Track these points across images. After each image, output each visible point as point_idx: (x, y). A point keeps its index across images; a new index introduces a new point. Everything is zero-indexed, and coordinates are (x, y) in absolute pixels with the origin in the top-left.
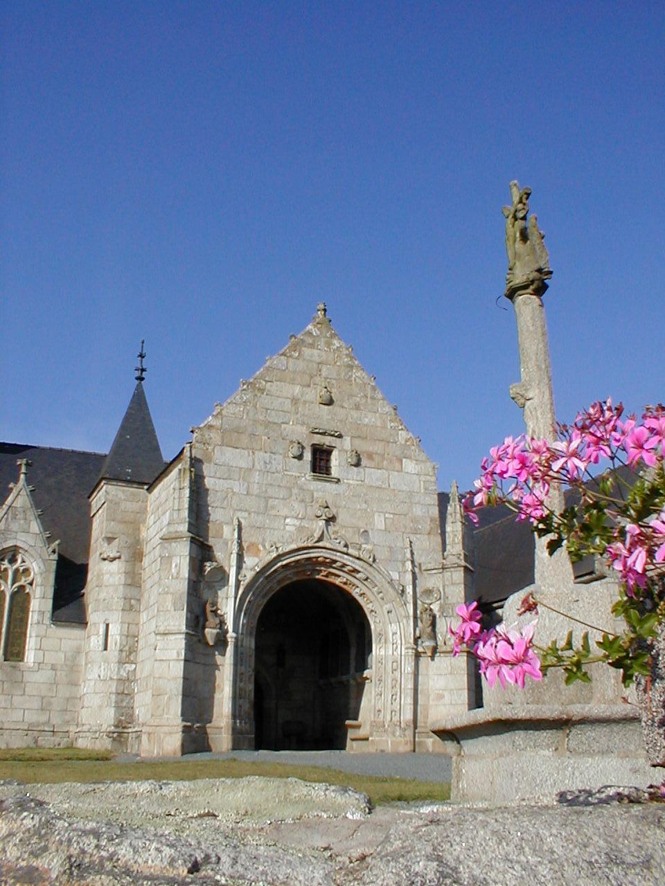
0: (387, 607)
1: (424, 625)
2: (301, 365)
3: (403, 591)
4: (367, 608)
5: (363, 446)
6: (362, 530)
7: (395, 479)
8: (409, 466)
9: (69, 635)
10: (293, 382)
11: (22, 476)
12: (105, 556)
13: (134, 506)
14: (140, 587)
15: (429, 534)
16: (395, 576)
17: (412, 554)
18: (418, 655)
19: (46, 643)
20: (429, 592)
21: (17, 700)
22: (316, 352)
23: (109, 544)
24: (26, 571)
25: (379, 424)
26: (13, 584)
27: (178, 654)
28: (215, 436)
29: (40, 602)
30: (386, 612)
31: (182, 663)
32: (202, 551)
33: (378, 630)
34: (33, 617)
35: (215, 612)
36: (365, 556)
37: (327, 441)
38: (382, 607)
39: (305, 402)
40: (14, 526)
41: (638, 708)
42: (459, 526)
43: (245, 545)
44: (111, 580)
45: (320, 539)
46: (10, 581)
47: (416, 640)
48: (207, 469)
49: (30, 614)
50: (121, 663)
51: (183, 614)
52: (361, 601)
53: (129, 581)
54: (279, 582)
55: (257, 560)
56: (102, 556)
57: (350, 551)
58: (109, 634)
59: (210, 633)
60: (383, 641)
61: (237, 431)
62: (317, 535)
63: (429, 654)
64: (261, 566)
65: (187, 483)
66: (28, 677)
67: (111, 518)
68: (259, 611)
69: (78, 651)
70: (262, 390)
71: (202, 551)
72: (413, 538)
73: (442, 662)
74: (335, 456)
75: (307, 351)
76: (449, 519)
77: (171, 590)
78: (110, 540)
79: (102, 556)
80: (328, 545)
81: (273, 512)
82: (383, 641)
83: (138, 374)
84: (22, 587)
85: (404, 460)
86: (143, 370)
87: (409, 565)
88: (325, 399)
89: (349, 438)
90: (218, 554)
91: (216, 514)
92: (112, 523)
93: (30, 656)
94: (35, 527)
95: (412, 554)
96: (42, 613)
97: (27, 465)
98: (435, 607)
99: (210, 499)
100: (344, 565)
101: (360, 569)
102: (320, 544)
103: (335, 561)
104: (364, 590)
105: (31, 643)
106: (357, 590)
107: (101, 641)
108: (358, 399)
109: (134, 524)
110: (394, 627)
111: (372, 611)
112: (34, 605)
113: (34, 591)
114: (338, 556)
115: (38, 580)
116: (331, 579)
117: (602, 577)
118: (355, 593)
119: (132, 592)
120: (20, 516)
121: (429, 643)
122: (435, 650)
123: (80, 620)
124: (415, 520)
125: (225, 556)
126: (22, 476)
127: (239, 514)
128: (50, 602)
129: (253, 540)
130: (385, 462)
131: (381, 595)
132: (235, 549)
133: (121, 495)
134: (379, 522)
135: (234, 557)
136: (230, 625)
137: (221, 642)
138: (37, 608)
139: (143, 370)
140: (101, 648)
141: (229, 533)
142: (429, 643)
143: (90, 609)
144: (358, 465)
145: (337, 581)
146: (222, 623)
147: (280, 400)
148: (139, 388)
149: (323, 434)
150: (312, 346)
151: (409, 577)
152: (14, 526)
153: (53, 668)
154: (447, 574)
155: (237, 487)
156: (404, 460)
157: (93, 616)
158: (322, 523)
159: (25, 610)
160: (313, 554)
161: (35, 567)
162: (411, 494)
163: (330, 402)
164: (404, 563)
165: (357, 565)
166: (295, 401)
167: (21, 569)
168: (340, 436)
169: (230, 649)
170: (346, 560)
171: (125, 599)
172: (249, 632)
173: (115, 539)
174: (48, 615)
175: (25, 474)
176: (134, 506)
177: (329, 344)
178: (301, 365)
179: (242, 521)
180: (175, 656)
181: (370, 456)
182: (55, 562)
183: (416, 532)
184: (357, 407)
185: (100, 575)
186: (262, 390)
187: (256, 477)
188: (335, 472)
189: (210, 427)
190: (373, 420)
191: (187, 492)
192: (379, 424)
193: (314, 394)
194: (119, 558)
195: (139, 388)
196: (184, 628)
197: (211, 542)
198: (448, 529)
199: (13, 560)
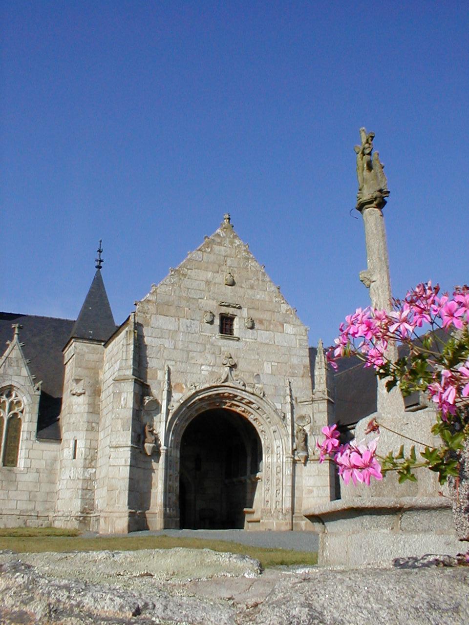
0: (273, 428)
1: (299, 441)
2: (212, 257)
3: (284, 417)
4: (259, 429)
5: (256, 315)
6: (255, 374)
7: (278, 338)
8: (289, 328)
9: (49, 448)
10: (206, 269)
11: (16, 336)
12: (74, 392)
13: (94, 357)
14: (99, 414)
15: (303, 376)
16: (279, 406)
17: (291, 391)
18: (295, 462)
19: (33, 454)
20: (302, 418)
21: (12, 494)
22: (223, 248)
23: (77, 384)
24: (19, 403)
25: (267, 299)
26: (9, 412)
27: (126, 461)
28: (152, 308)
29: (28, 424)
30: (272, 432)
31: (128, 468)
32: (142, 389)
33: (267, 444)
34: (23, 436)
35: (151, 432)
36: (257, 392)
37: (231, 311)
38: (269, 428)
39: (215, 284)
40: (10, 371)
42: (324, 371)
43: (173, 384)
44: (78, 409)
45: (226, 380)
46: (7, 410)
47: (293, 451)
48: (146, 331)
49: (21, 433)
50: (85, 467)
51: (129, 433)
52: (255, 424)
53: (91, 410)
54: (197, 410)
55: (181, 395)
56: (72, 392)
57: (247, 389)
58: (77, 447)
59: (148, 447)
60: (270, 452)
61: (167, 304)
62: (223, 378)
63: (303, 461)
64: (184, 399)
65: (132, 341)
66: (20, 478)
67: (78, 365)
68: (183, 431)
69: (55, 460)
70: (185, 275)
71: (142, 389)
72: (292, 380)
73: (312, 467)
74: (236, 322)
75: (216, 248)
76: (317, 366)
77: (121, 416)
78: (77, 381)
79: (72, 392)
80: (231, 385)
81: (193, 361)
82: (270, 452)
83: (97, 264)
84: (15, 414)
86: (101, 261)
87: (288, 399)
89: (246, 309)
90: (154, 391)
91: (153, 363)
92: (79, 369)
93: (21, 463)
94: (25, 371)
95: (291, 391)
96: (29, 432)
97: (19, 328)
98: (307, 429)
99: (148, 352)
100: (243, 399)
101: (254, 401)
102: (226, 384)
103: (236, 396)
104: (257, 416)
105: (22, 454)
106: (252, 416)
107: (71, 452)
108: (253, 282)
109: (95, 370)
110: (278, 443)
111: (262, 431)
112: (24, 427)
113: (24, 417)
114: (238, 392)
115: (27, 409)
116: (234, 409)
117: (425, 407)
118: (251, 418)
119: (93, 418)
120: (14, 364)
121: (303, 454)
122: (307, 459)
123: (56, 438)
124: (293, 367)
125: (159, 392)
126: (16, 336)
127: (168, 363)
128: (35, 425)
129: (179, 381)
130: (272, 326)
131: (269, 419)
132: (166, 387)
133: (85, 349)
134: (267, 368)
135: (165, 393)
136: (162, 441)
137: (156, 453)
138: (26, 429)
139: (101, 261)
140: (71, 457)
141: (162, 376)
142: (303, 454)
143: (63, 430)
144: (252, 328)
145: (238, 410)
146: (157, 440)
147: (197, 282)
148: (98, 274)
149: (228, 306)
150: (220, 244)
151: (289, 407)
152: (10, 371)
153: (38, 471)
154: (315, 405)
155: (167, 344)
156: (285, 325)
157: (66, 435)
158: (227, 369)
159: (18, 430)
160: (221, 391)
161: (25, 400)
162: (290, 348)
164: (285, 397)
165: (252, 398)
166: (208, 283)
167: (15, 401)
168: (240, 308)
169: (162, 458)
170: (244, 395)
171: (88, 422)
173: (81, 380)
174: (34, 434)
175: (18, 334)
176: (94, 357)
177: (232, 243)
178: (212, 257)
179: (171, 367)
180: (123, 463)
181: (261, 322)
182: (39, 396)
183: (293, 375)
184: (252, 287)
185: (71, 406)
186: (185, 275)
187: (181, 336)
188: (236, 333)
189: (148, 301)
190: (263, 296)
192: (267, 299)
193: (221, 278)
194: (84, 393)
195: (98, 274)
196: (129, 443)
197: (149, 382)
198: (316, 373)
199: (9, 395)
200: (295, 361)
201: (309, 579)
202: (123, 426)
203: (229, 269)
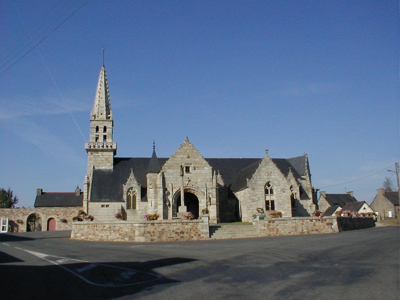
1: (208, 199)
2: (183, 151)
3: (204, 193)
4: (198, 197)
5: (196, 165)
7: (203, 171)
8: (206, 168)
9: (144, 203)
10: (181, 154)
13: (155, 177)
16: (203, 190)
17: (206, 186)
18: (207, 205)
19: (140, 206)
20: (209, 193)
21: (136, 217)
22: (186, 147)
25: (199, 160)
26: (133, 193)
28: (166, 167)
29: (138, 197)
32: (165, 189)
34: (137, 200)
35: (168, 200)
36: (196, 187)
37: (188, 165)
39: (184, 158)
40: (132, 183)
41: (309, 221)
43: (173, 187)
44: (152, 193)
45: (188, 185)
47: (207, 203)
48: (165, 174)
50: (155, 209)
51: (162, 201)
52: (197, 195)
55: (175, 190)
57: (194, 186)
59: (167, 204)
61: (171, 166)
62: (187, 184)
63: (209, 205)
64: (177, 191)
65: (162, 178)
66: (138, 212)
67: (150, 180)
69: (147, 206)
70: (175, 157)
71: (165, 189)
72: (206, 183)
73: (212, 206)
74: (190, 168)
75: (184, 147)
76: (213, 179)
78: (150, 185)
80: (189, 186)
81: (178, 180)
83: (153, 148)
85: (205, 167)
87: (205, 188)
88: (188, 156)
89: (193, 164)
90: (168, 189)
91: (167, 182)
93: (137, 208)
94: (136, 182)
95: (206, 186)
97: (133, 170)
98: (210, 196)
99: (166, 180)
102: (188, 186)
103: (190, 189)
105: (137, 206)
107: (151, 205)
109: (155, 181)
110: (203, 200)
112: (137, 198)
114: (191, 188)
116: (191, 192)
117: (248, 187)
118: (195, 194)
119: (156, 195)
120: (133, 180)
121: (209, 203)
122: (210, 204)
123: (146, 200)
124: (207, 179)
125: (169, 190)
127: (172, 182)
128: (140, 197)
129: (175, 186)
132: (171, 188)
133: (152, 175)
134: (199, 180)
135: (171, 190)
136: (171, 202)
137: (169, 205)
140: (151, 206)
141: (170, 185)
142: (209, 203)
143: (148, 198)
144: (195, 169)
145: (192, 192)
146: (169, 202)
147: (179, 159)
149: (188, 164)
150: (185, 146)
151: (205, 190)
152: (132, 183)
153: (142, 210)
154: (213, 190)
155: (171, 177)
156: (205, 167)
157: (148, 200)
158: (188, 182)
159: (135, 199)
160: (186, 188)
161: (136, 190)
162: (206, 174)
163: (189, 157)
164: (204, 188)
165: (195, 189)
166: (182, 158)
168: (191, 164)
169: (171, 206)
170: (193, 188)
172: (82, 207)
174: (140, 200)
176: (155, 177)
177: (188, 145)
178: (183, 151)
179: (173, 183)
181: (197, 167)
183: (207, 181)
184: (195, 158)
185: (149, 192)
186: (175, 157)
187: (175, 174)
188: (190, 172)
189: (165, 166)
191: (162, 179)
192: (199, 160)
193: (186, 156)
195: (154, 150)
196: (162, 203)
197: (166, 187)
199: (132, 189)
200: (208, 177)
201: (141, 218)
202: (161, 199)
203: (191, 148)
